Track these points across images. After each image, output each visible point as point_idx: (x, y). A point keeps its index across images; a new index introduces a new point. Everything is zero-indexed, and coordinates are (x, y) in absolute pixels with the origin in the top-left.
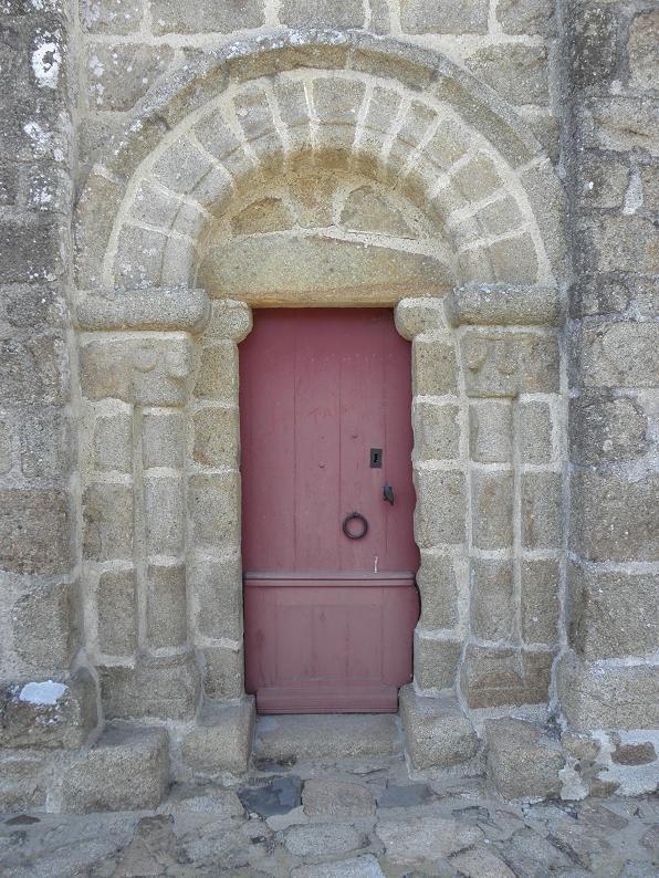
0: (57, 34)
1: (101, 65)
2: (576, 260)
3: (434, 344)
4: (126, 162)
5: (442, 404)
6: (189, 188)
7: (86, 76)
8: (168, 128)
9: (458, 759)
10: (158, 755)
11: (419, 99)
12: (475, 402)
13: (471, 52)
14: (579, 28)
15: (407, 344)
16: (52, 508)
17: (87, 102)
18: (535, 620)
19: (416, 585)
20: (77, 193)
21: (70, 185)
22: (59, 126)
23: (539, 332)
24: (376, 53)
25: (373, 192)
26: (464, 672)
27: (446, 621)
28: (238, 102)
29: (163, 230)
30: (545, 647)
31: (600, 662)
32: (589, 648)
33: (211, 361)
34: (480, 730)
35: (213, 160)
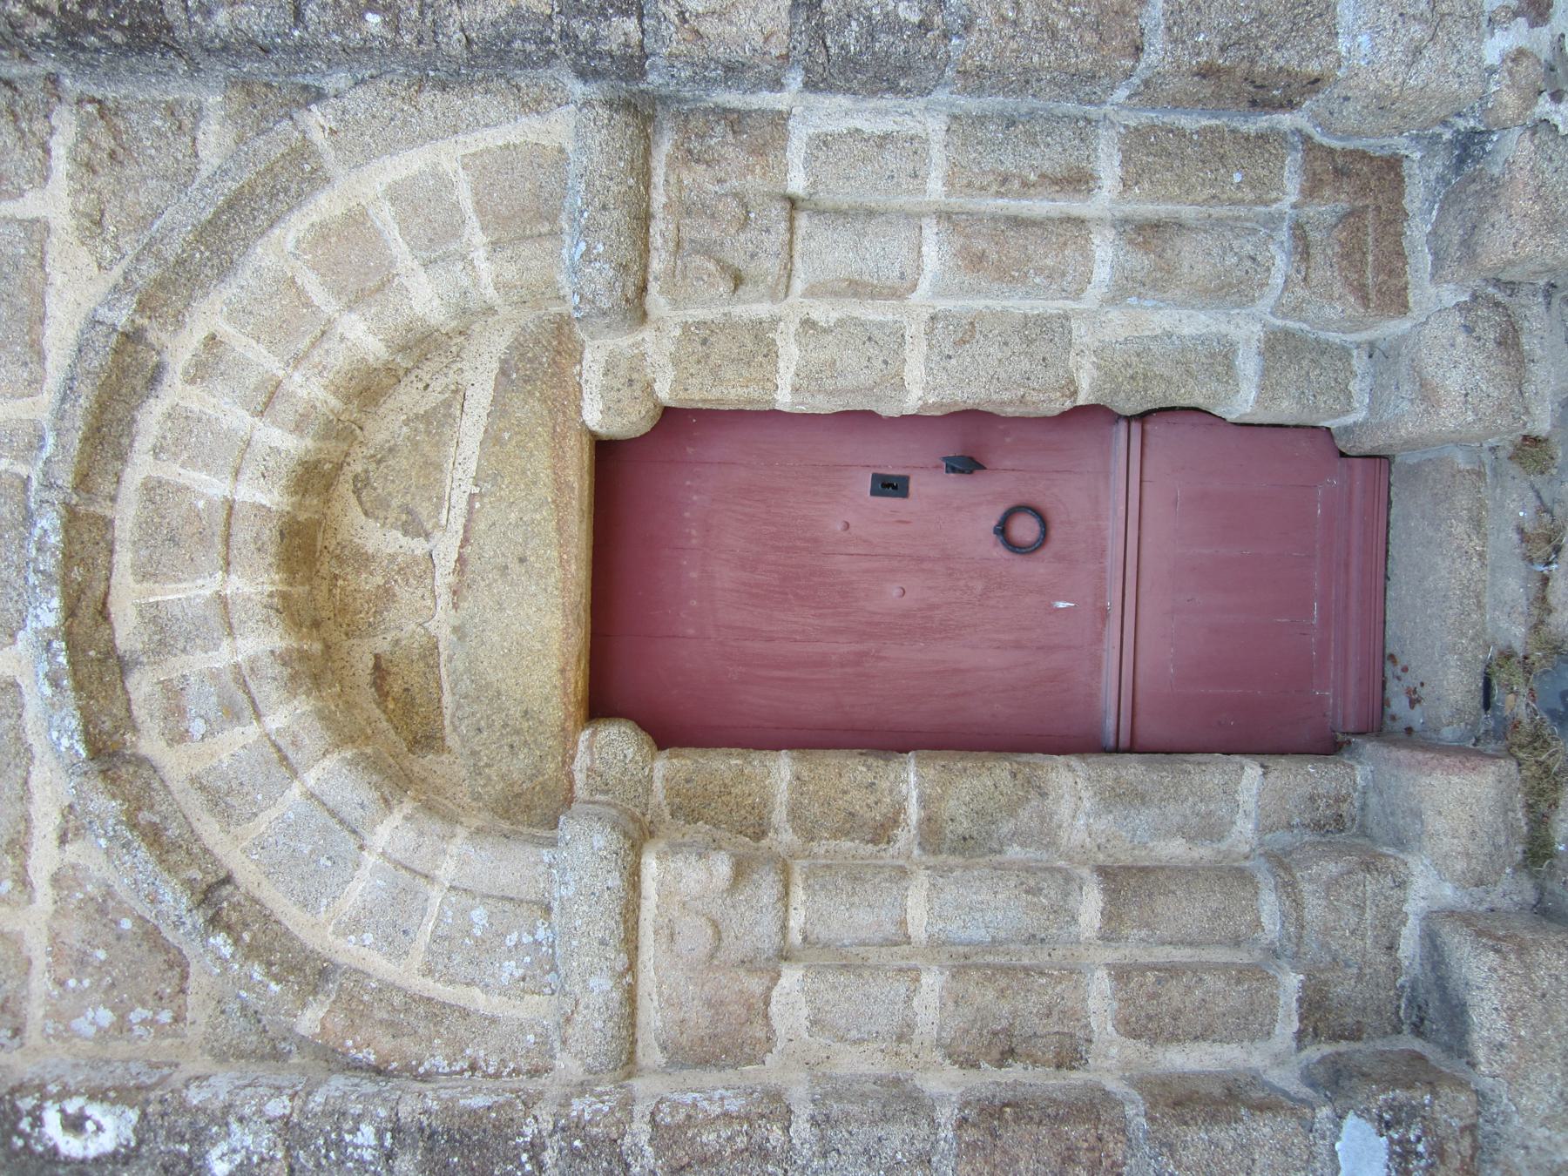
0: (26, 1103)
1: (90, 1014)
2: (526, 62)
3: (676, 362)
4: (296, 968)
5: (794, 350)
6: (352, 843)
7: (113, 1044)
8: (228, 880)
9: (1509, 340)
10: (1491, 936)
11: (179, 370)
12: (798, 285)
13: (84, 256)
14: (42, 26)
15: (671, 420)
16: (994, 1134)
17: (167, 1042)
18: (1237, 178)
19: (1143, 417)
20: (355, 1067)
21: (338, 1083)
22: (217, 1105)
23: (665, 147)
24: (82, 451)
25: (366, 471)
26: (1327, 325)
27: (1222, 358)
28: (178, 737)
29: (436, 895)
30: (1293, 161)
31: (1343, 45)
32: (1314, 68)
33: (695, 803)
34: (1451, 295)
35: (295, 791)
